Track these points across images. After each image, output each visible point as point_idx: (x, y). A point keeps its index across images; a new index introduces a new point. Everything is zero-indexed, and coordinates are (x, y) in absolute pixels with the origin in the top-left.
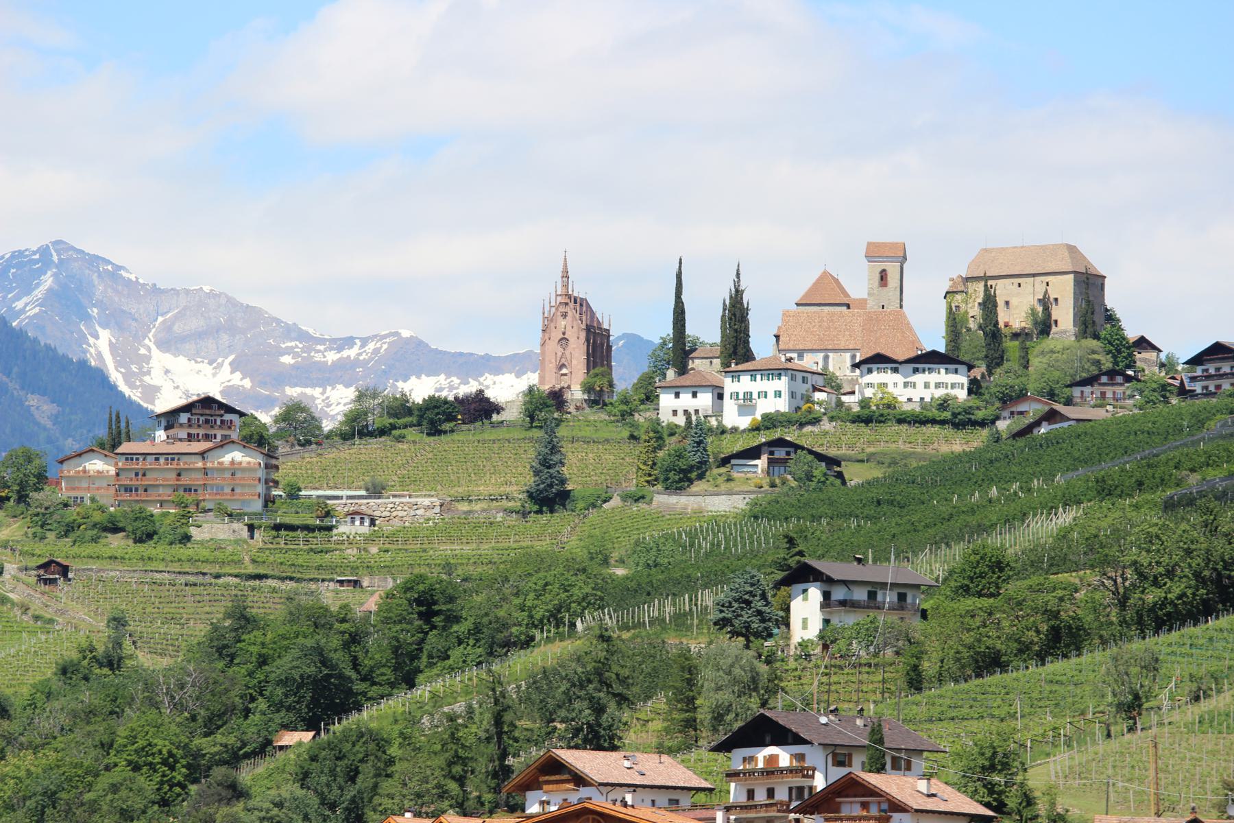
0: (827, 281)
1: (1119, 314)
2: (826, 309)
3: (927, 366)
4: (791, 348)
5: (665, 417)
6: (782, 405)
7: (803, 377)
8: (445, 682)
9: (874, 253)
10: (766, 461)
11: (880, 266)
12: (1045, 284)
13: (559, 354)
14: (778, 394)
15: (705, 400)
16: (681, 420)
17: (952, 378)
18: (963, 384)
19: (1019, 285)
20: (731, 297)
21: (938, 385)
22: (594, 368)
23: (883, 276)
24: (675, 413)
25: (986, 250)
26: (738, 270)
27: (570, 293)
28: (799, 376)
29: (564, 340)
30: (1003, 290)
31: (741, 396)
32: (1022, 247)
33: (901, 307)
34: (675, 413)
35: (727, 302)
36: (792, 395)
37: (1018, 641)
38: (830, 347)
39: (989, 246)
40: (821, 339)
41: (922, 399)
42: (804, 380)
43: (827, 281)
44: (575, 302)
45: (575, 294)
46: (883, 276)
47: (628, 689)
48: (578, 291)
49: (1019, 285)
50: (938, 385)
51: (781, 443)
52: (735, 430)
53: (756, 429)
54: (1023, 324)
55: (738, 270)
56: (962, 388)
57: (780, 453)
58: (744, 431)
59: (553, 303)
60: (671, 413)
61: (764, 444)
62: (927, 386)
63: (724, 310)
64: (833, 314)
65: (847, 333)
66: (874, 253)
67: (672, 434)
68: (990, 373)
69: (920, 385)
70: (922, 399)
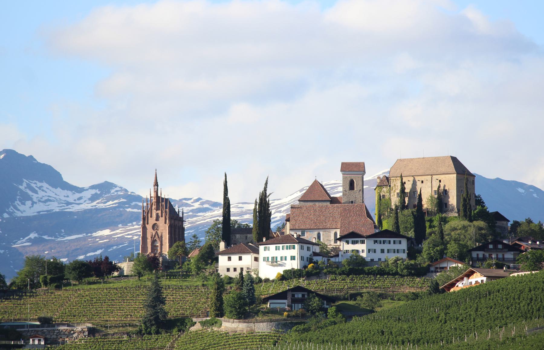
0: (317, 186)
1: (484, 199)
2: (317, 204)
3: (382, 239)
4: (297, 228)
6: (295, 265)
7: (308, 247)
8: (535, 256)
9: (346, 167)
10: (290, 300)
11: (349, 177)
12: (438, 181)
14: (293, 258)
17: (397, 247)
18: (404, 250)
19: (422, 182)
22: (175, 242)
23: (352, 184)
24: (228, 270)
25: (401, 160)
26: (267, 181)
27: (159, 195)
28: (305, 246)
31: (270, 260)
32: (423, 158)
33: (363, 202)
34: (228, 270)
35: (258, 201)
36: (302, 258)
37: (537, 311)
38: (321, 227)
39: (402, 158)
40: (315, 223)
42: (308, 249)
43: (317, 186)
45: (163, 196)
46: (352, 184)
48: (165, 194)
49: (422, 182)
51: (298, 289)
52: (267, 280)
53: (283, 278)
55: (267, 181)
56: (404, 252)
57: (299, 295)
58: (273, 281)
61: (289, 290)
62: (382, 251)
63: (256, 205)
64: (322, 207)
65: (331, 219)
66: (346, 167)
67: (229, 283)
69: (378, 251)
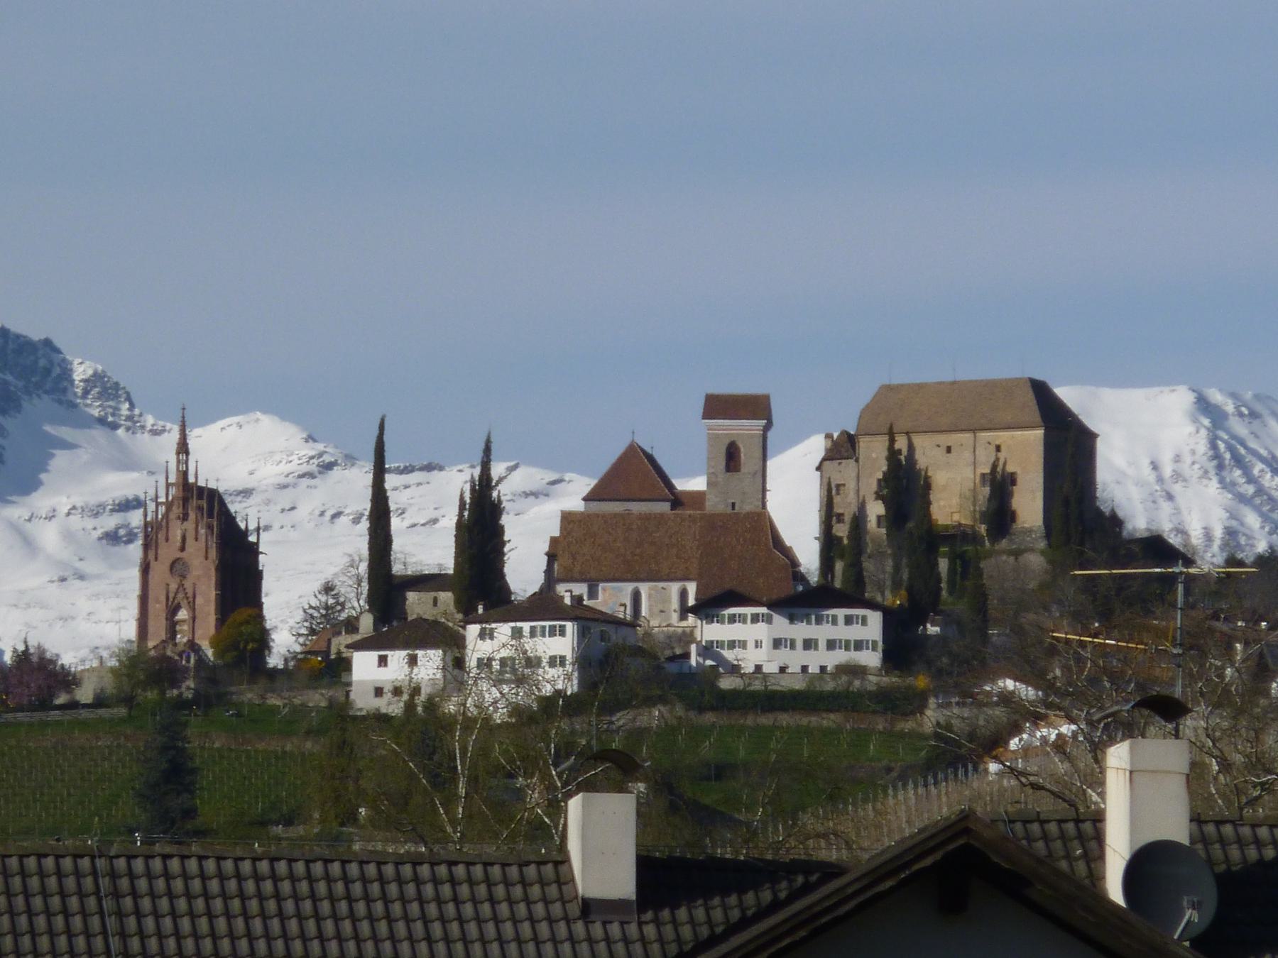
5: (363, 701)
12: (993, 448)
13: (173, 587)
15: (430, 664)
16: (394, 708)
19: (949, 450)
20: (473, 490)
21: (831, 645)
29: (179, 568)
30: (927, 453)
31: (496, 666)
34: (379, 692)
41: (805, 669)
44: (200, 497)
45: (201, 483)
47: (363, 578)
49: (949, 450)
50: (831, 645)
54: (956, 517)
56: (874, 649)
59: (162, 499)
60: (372, 693)
68: (893, 454)
70: (805, 669)
